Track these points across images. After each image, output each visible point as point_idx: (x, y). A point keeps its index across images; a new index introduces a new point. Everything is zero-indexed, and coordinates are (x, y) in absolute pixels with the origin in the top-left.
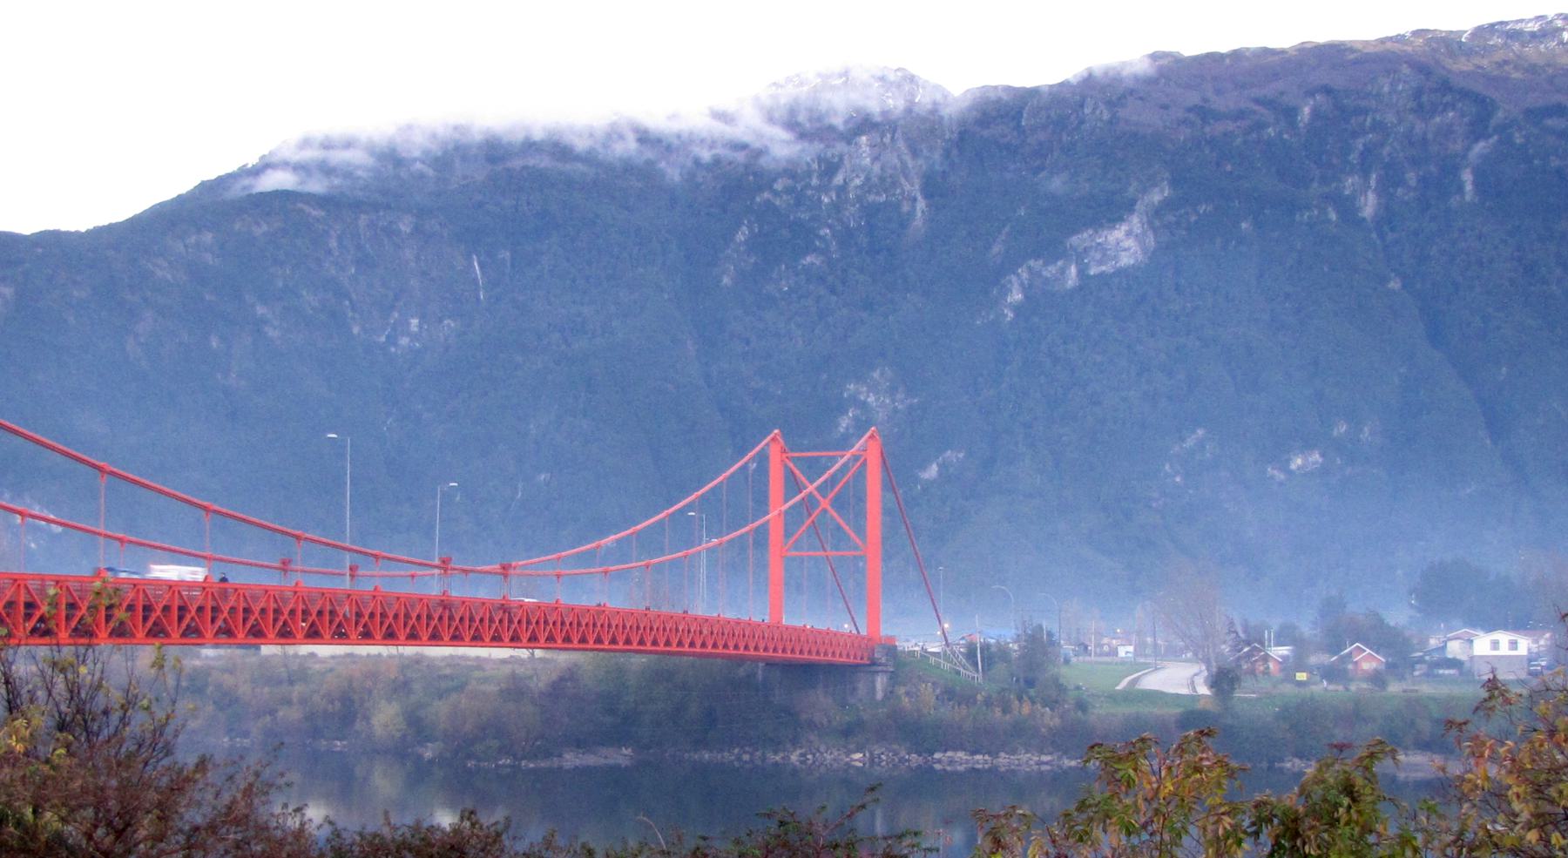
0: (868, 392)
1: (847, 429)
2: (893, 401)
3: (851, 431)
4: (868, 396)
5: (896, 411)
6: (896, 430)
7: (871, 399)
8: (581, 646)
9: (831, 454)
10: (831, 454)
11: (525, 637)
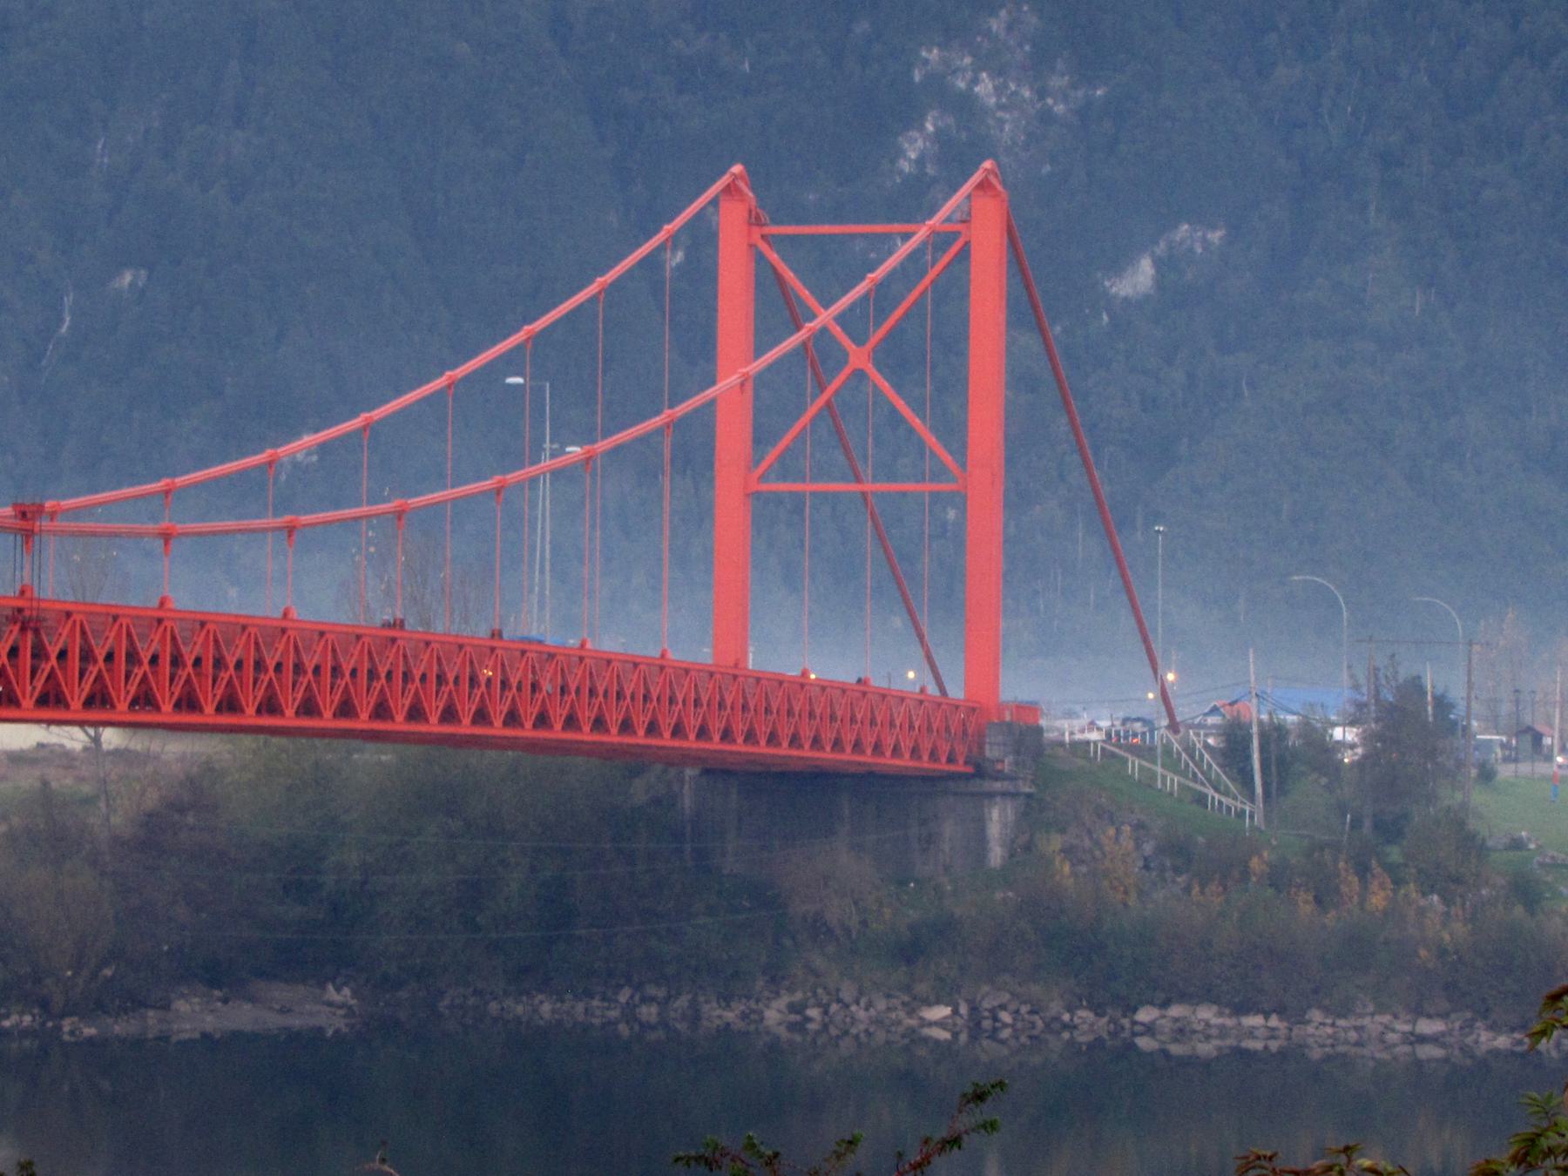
0: (977, 70)
1: (920, 162)
2: (1042, 94)
3: (930, 170)
4: (975, 81)
5: (1046, 117)
6: (1047, 169)
7: (985, 87)
8: (306, 722)
9: (878, 228)
10: (878, 228)
11: (77, 695)
